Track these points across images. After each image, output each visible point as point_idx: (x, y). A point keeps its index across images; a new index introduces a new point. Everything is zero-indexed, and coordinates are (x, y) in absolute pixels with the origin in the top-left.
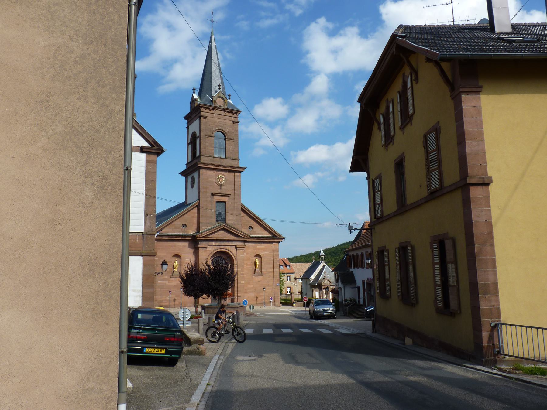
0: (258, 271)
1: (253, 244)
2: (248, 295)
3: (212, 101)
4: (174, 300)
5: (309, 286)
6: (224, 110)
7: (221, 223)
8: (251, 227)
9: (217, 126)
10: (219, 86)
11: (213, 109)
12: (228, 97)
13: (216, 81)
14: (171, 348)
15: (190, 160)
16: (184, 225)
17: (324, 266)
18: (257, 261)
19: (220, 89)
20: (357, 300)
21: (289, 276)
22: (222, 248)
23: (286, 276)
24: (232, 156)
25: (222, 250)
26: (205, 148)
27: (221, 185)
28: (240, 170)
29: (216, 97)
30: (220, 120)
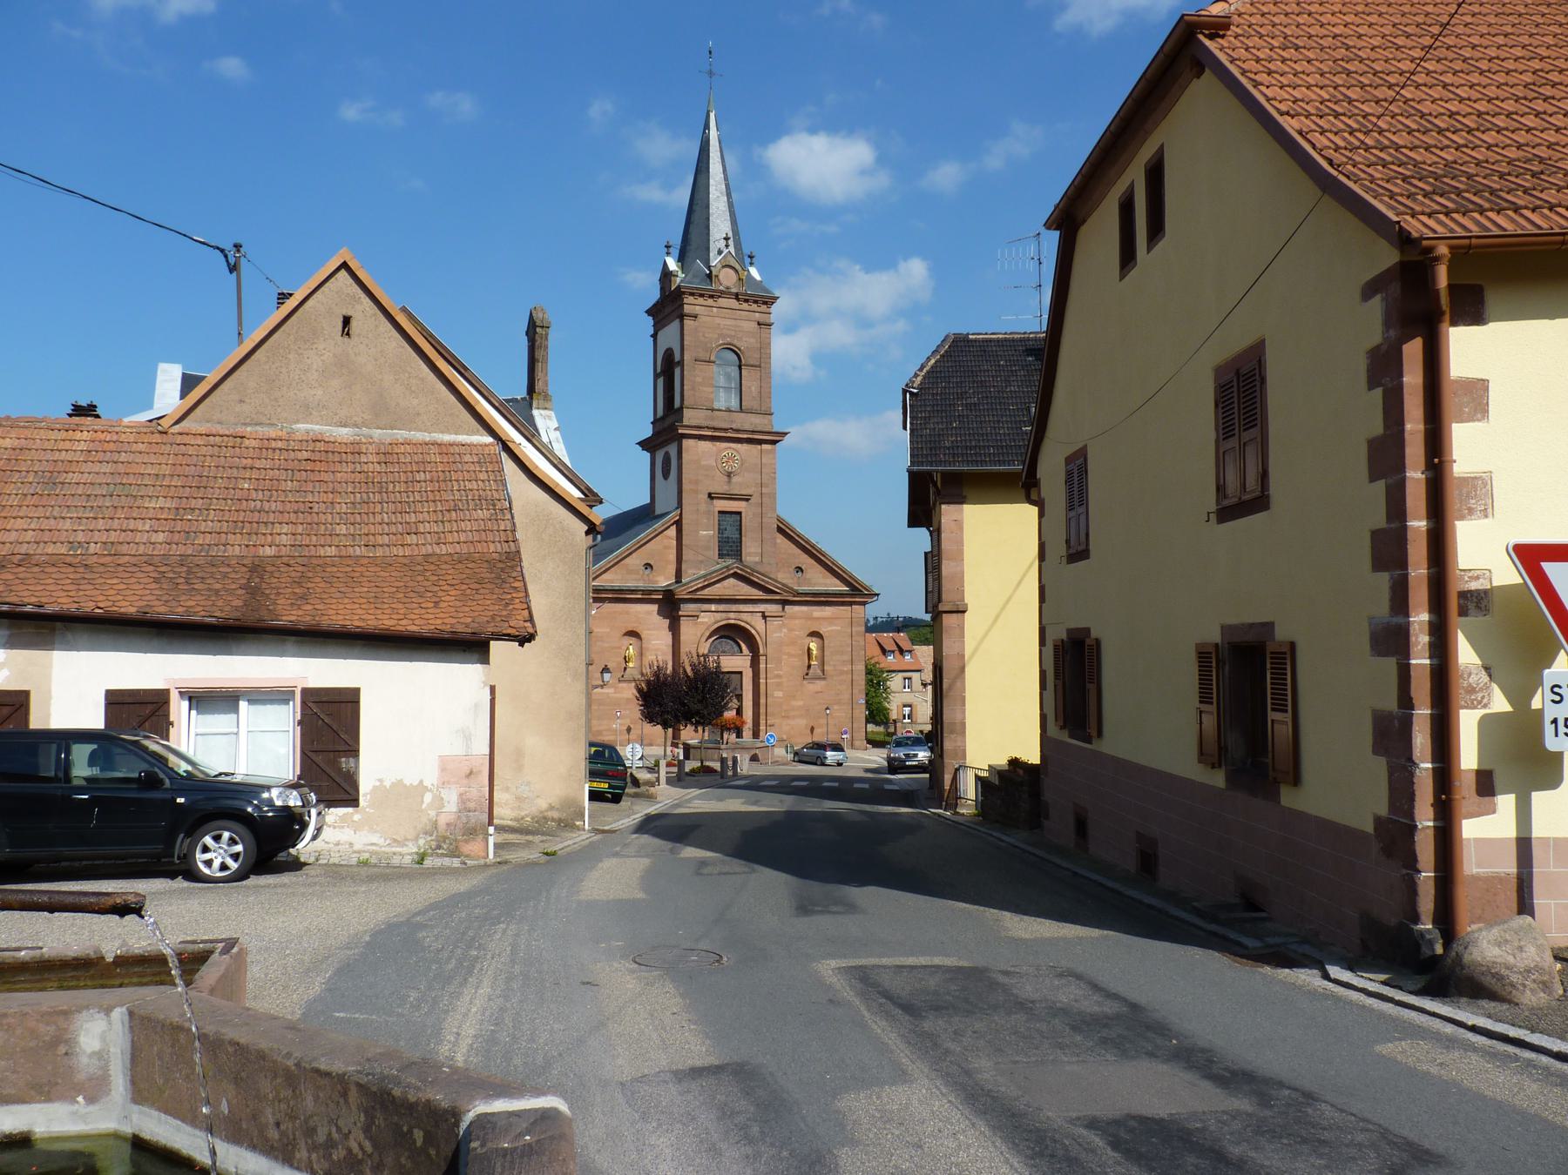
0: (816, 670)
1: (804, 608)
3: (710, 276)
4: (629, 730)
6: (737, 297)
7: (730, 561)
8: (799, 569)
9: (721, 336)
10: (727, 239)
11: (711, 297)
12: (748, 261)
13: (720, 225)
14: (614, 782)
15: (660, 413)
16: (648, 566)
18: (813, 646)
24: (755, 405)
26: (693, 389)
28: (775, 438)
30: (729, 322)
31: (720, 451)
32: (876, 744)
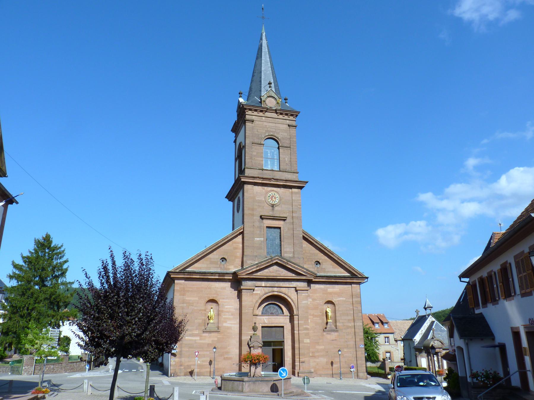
0: (331, 325)
2: (317, 360)
5: (413, 350)
6: (276, 111)
10: (270, 83)
11: (261, 111)
16: (223, 259)
17: (433, 323)
18: (329, 310)
19: (270, 87)
20: (502, 375)
21: (388, 337)
22: (276, 292)
23: (382, 336)
24: (288, 168)
25: (276, 293)
26: (251, 158)
27: (273, 206)
29: (266, 96)
31: (267, 192)
32: (373, 374)
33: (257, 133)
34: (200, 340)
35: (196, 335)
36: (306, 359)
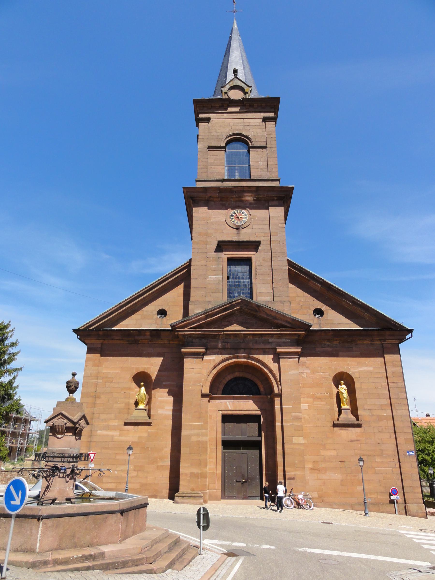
27: (238, 228)
33: (215, 134)
34: (120, 435)
35: (114, 428)
36: (298, 473)
